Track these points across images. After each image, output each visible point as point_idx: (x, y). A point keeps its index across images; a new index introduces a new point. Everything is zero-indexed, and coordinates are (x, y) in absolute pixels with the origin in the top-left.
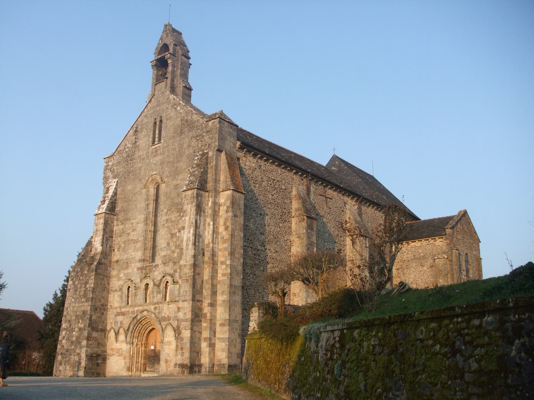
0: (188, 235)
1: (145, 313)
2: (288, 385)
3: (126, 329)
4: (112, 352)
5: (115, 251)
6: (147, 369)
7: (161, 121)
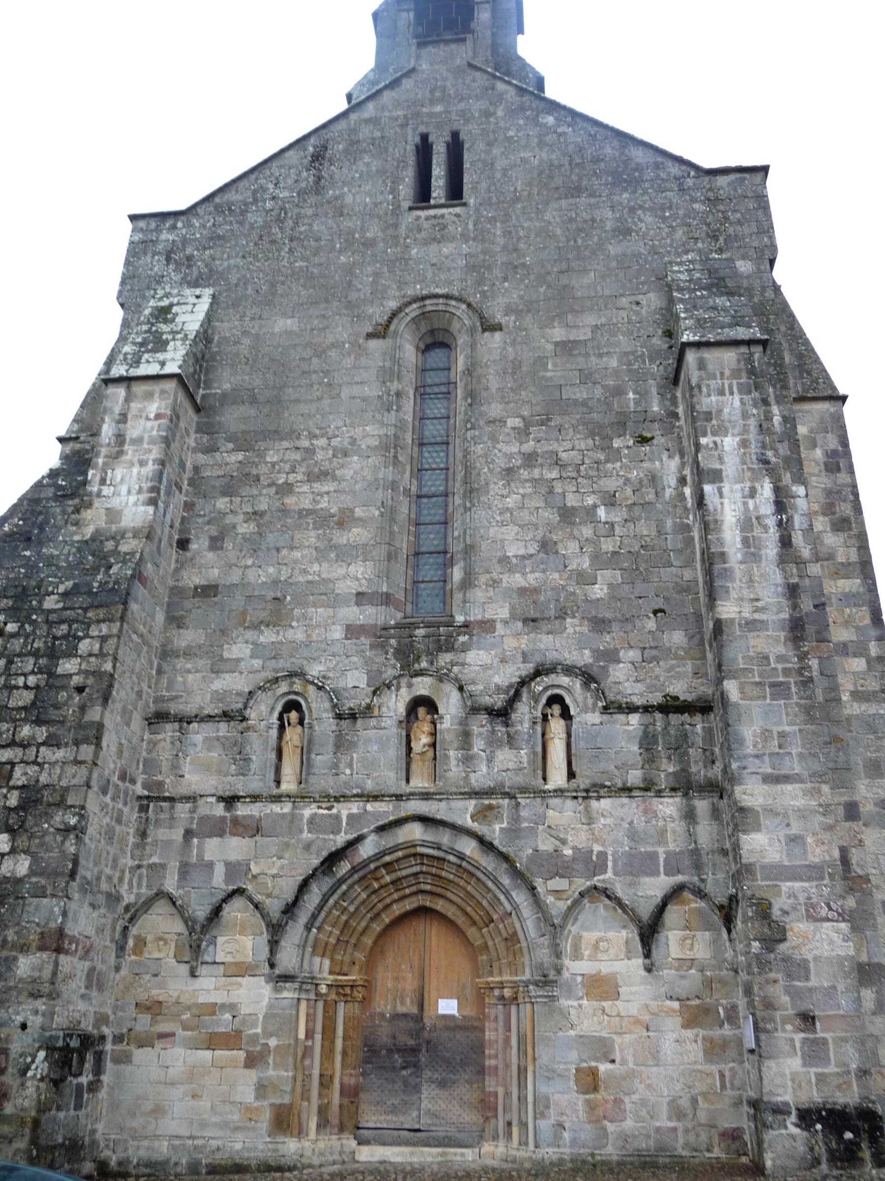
0: (745, 504)
1: (415, 832)
2: (281, 1106)
3: (274, 907)
4: (154, 1022)
5: (193, 546)
6: (371, 1118)
7: (456, 149)
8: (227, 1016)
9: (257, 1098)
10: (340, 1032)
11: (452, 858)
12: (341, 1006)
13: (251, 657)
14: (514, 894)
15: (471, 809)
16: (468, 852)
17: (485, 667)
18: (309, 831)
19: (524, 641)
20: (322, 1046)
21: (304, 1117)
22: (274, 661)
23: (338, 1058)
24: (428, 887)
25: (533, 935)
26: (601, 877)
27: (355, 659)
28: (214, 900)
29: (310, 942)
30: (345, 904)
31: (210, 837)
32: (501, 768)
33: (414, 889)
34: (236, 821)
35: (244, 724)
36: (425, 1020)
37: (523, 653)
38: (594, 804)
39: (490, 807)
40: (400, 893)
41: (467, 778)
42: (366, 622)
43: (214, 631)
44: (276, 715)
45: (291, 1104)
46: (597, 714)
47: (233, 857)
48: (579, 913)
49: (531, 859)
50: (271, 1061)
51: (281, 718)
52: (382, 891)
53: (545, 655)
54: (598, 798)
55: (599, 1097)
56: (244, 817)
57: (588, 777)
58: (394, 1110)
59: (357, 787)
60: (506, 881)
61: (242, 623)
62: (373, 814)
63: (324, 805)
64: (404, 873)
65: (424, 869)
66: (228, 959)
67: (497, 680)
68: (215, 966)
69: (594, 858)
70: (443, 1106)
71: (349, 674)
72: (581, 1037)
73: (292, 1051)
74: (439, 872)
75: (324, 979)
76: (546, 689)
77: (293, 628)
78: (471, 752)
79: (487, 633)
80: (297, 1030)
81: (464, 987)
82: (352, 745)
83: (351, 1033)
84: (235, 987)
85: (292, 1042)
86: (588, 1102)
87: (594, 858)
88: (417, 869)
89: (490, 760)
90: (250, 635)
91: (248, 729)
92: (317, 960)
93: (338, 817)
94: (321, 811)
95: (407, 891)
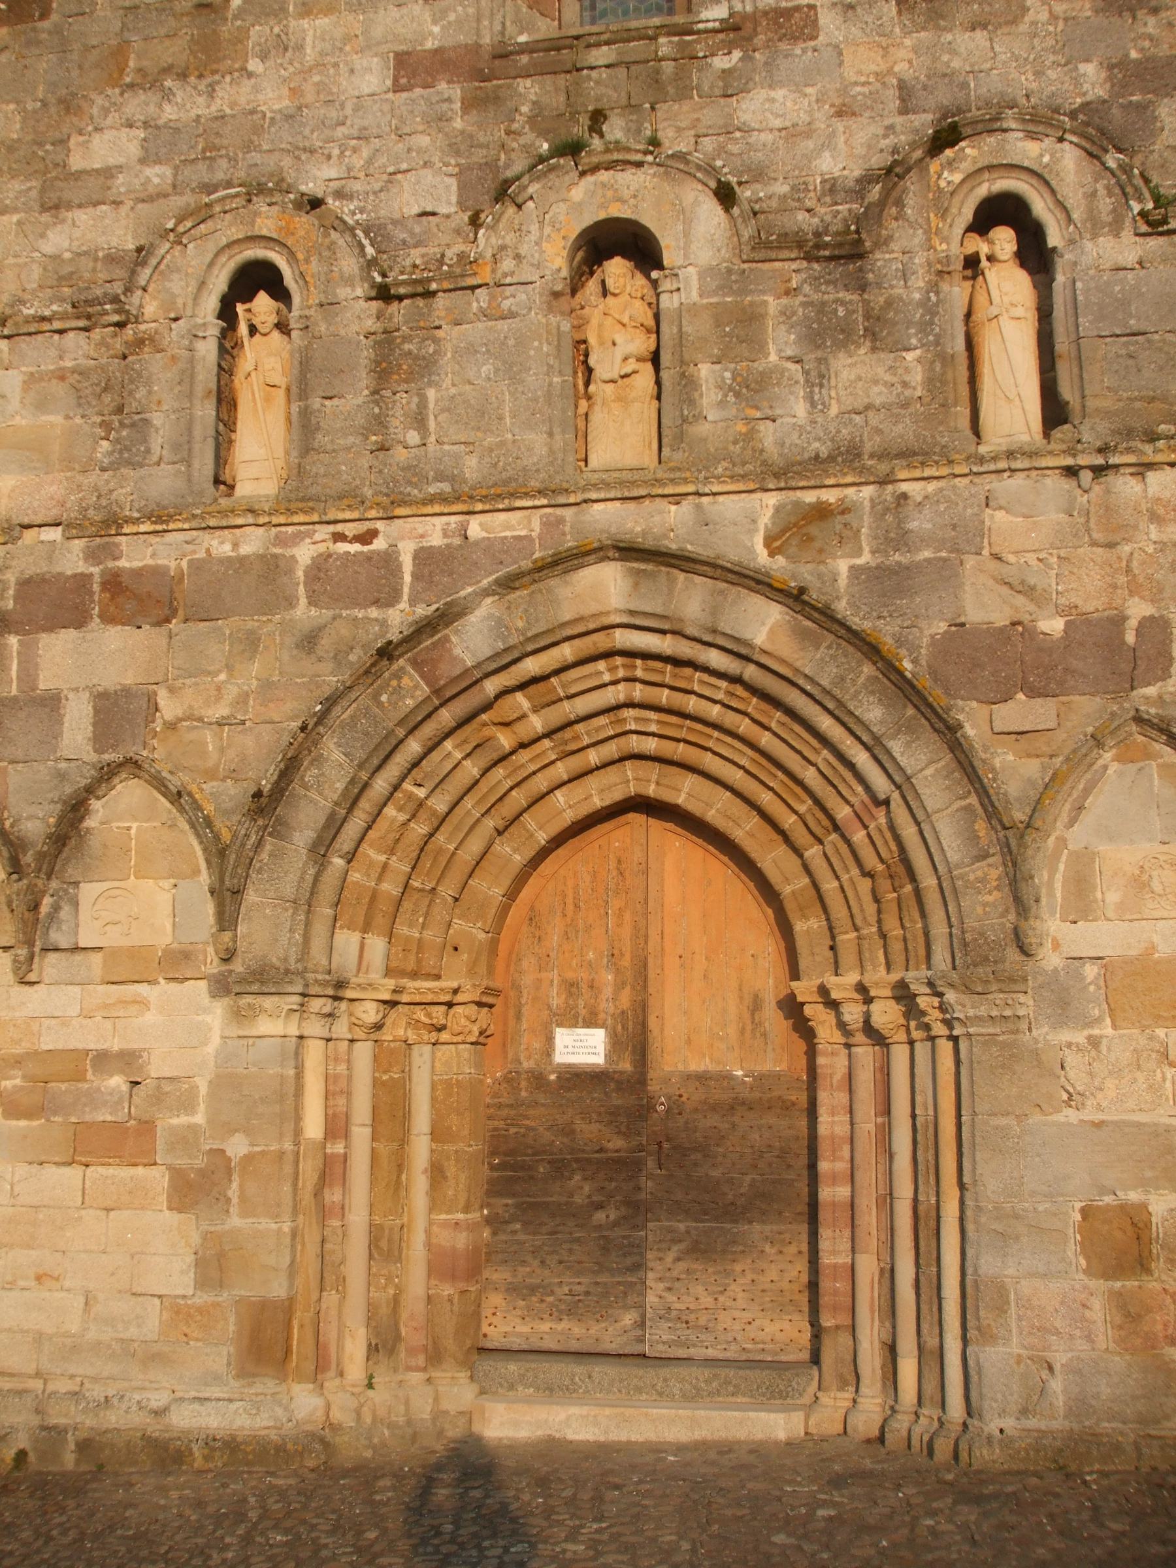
2: (264, 1305)
8: (117, 1082)
9: (202, 1283)
10: (422, 1121)
11: (715, 659)
12: (422, 1057)
13: (143, 161)
14: (896, 746)
15: (765, 519)
16: (760, 638)
17: (792, 133)
18: (313, 602)
19: (902, 53)
20: (374, 1156)
21: (330, 1333)
22: (202, 166)
23: (420, 1184)
24: (651, 745)
25: (953, 856)
26: (1151, 691)
27: (424, 141)
28: (68, 790)
29: (327, 890)
30: (421, 793)
31: (50, 629)
32: (849, 403)
33: (611, 750)
34: (114, 584)
35: (129, 331)
36: (653, 1087)
37: (902, 86)
38: (1126, 487)
39: (822, 512)
40: (575, 764)
41: (750, 436)
42: (449, 42)
43: (45, 104)
44: (211, 303)
45: (291, 1300)
46: (1127, 235)
47: (112, 677)
48: (1087, 792)
49: (944, 647)
50: (233, 1191)
51: (227, 312)
52: (524, 756)
53: (964, 86)
54: (1143, 468)
55: (1154, 1285)
56: (138, 573)
57: (1107, 414)
58: (572, 1309)
59: (440, 477)
60: (873, 712)
61: (114, 80)
62: (487, 546)
63: (350, 530)
64: (582, 705)
65: (638, 692)
66: (113, 938)
67: (829, 165)
68: (78, 957)
69: (1130, 638)
70: (707, 1301)
71: (405, 180)
72: (1099, 1125)
73: (288, 1169)
74: (678, 700)
75: (371, 986)
76: (973, 176)
77: (250, 75)
78: (760, 366)
79: (794, 39)
80: (298, 1118)
81: (756, 1005)
82: (425, 368)
83: (454, 1121)
84: (133, 1009)
85: (288, 1146)
86: (1120, 1301)
87: (1130, 638)
88: (619, 693)
89: (818, 379)
90: (138, 105)
91: (140, 343)
92: (347, 941)
93: (389, 560)
94: (343, 547)
95: (593, 757)
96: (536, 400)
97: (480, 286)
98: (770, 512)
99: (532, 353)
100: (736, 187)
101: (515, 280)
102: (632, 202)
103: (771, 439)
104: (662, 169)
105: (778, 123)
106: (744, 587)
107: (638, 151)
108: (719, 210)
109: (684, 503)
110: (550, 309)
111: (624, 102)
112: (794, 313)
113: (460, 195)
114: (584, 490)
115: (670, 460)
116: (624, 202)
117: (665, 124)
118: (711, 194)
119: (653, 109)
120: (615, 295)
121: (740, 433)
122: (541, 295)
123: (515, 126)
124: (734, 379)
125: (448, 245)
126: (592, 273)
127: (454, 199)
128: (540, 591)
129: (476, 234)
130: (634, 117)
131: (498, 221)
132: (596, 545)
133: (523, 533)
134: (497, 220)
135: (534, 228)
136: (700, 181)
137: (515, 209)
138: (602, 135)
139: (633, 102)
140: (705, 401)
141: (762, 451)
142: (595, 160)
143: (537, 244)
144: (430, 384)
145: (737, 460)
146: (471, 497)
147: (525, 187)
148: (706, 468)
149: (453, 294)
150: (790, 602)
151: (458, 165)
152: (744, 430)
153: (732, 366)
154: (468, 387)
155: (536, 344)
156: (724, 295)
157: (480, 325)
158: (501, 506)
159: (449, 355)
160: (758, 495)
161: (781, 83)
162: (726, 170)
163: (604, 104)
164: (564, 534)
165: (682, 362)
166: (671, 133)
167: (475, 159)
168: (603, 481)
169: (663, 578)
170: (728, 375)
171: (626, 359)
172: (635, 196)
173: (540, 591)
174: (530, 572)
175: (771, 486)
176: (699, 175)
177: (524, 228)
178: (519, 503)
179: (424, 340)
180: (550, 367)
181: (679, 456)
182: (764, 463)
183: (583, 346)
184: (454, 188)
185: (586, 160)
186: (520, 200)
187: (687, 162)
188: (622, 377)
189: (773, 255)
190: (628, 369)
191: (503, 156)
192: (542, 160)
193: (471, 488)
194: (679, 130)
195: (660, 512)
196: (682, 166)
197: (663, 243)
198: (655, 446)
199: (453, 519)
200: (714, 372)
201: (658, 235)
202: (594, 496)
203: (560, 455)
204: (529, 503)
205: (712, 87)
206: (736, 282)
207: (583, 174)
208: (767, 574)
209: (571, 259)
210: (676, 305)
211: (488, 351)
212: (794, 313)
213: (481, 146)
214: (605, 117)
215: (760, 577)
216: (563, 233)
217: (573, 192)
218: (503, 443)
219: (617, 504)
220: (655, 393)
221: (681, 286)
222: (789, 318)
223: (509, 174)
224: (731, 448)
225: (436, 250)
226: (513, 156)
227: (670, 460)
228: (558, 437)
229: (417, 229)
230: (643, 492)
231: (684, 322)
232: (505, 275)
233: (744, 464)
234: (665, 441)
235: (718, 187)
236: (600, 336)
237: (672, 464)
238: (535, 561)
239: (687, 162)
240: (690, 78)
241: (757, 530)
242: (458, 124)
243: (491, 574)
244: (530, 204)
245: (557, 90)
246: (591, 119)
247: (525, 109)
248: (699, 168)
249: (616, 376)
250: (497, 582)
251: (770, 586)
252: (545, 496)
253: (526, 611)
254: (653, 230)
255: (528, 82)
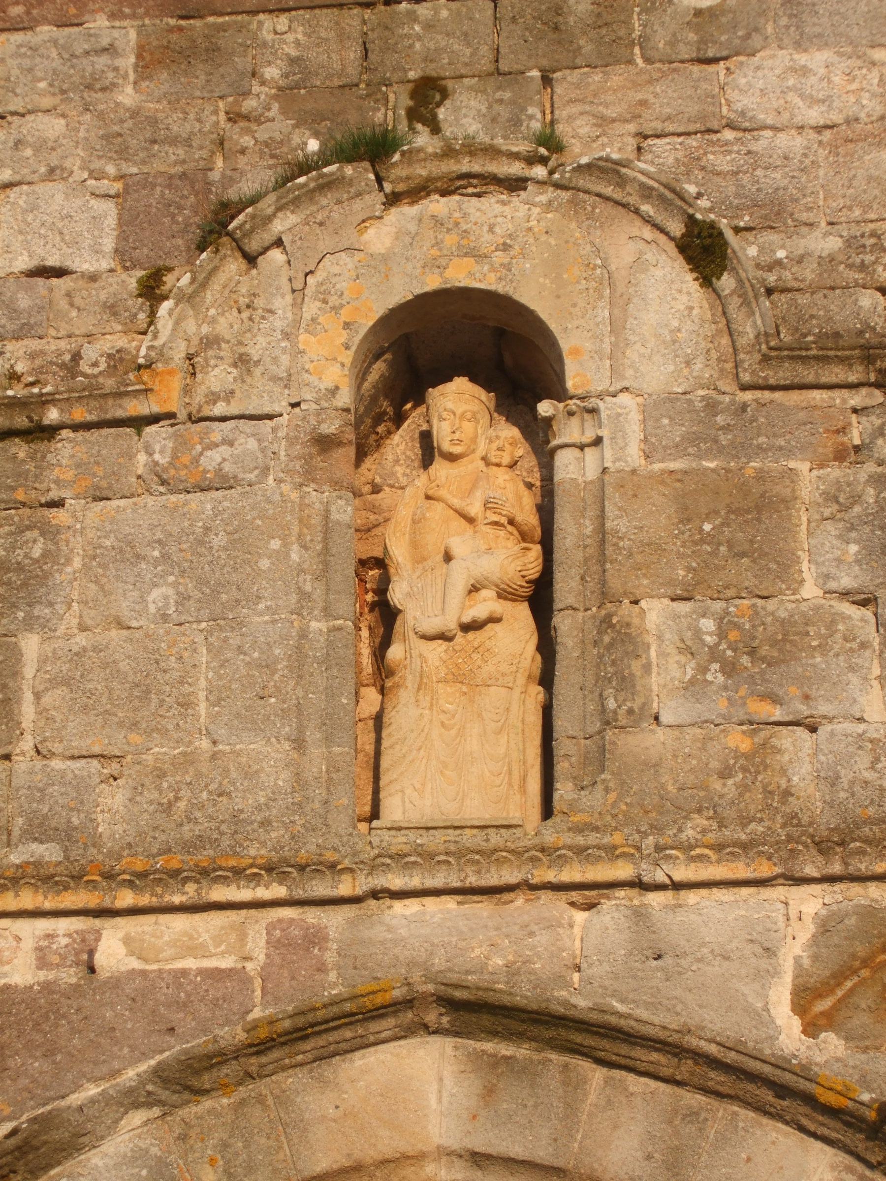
27: (53, 127)
96: (269, 666)
97: (154, 419)
98: (806, 932)
99: (264, 564)
100: (729, 234)
101: (234, 410)
102: (499, 257)
103: (806, 768)
104: (565, 195)
105: (815, 115)
106: (747, 1104)
107: (516, 156)
108: (689, 282)
109: (607, 905)
110: (309, 475)
111: (485, 64)
112: (856, 499)
113: (122, 237)
114: (373, 868)
115: (573, 807)
116: (480, 257)
117: (574, 109)
118: (671, 247)
119: (547, 81)
120: (452, 458)
121: (737, 754)
122: (291, 441)
123: (249, 104)
124: (722, 634)
125: (89, 336)
126: (399, 419)
127: (109, 243)
128: (261, 1100)
129: (152, 314)
130: (507, 95)
131: (204, 285)
132: (397, 993)
133: (226, 963)
134: (202, 284)
135: (282, 303)
136: (648, 221)
137: (242, 263)
138: (435, 129)
139: (504, 66)
140: (654, 680)
141: (787, 793)
142: (422, 171)
143: (286, 336)
144: (29, 624)
145: (730, 813)
146: (109, 876)
147: (269, 219)
148: (656, 828)
149: (94, 435)
150: (858, 1141)
151: (121, 177)
152: (745, 745)
153: (719, 606)
154: (114, 633)
155: (275, 544)
156: (699, 457)
157: (150, 500)
158: (177, 899)
159: (77, 563)
160: (779, 892)
161: (821, 41)
162: (703, 203)
163: (441, 67)
164: (322, 969)
165: (605, 596)
166: (584, 126)
167: (158, 166)
168: (419, 851)
169: (552, 1079)
170: (708, 625)
171: (474, 589)
172: (506, 247)
173: (261, 1100)
174: (238, 1053)
175: (810, 870)
176: (646, 208)
177: (259, 302)
178: (219, 893)
179: (22, 530)
180: (304, 596)
181: (594, 799)
182: (792, 819)
183: (374, 573)
184: (111, 221)
185: (401, 172)
186: (253, 245)
187: (622, 182)
188: (466, 628)
189: (809, 375)
190: (480, 610)
191: (219, 163)
192: (304, 168)
193: (110, 854)
194: (603, 122)
195: (551, 925)
196: (608, 191)
197: (565, 344)
198: (534, 785)
199: (64, 925)
200: (676, 617)
201: (553, 326)
202: (396, 882)
203: (318, 793)
204: (245, 894)
205: (673, 43)
206: (726, 428)
207: (393, 200)
208: (805, 1072)
209: (361, 376)
210: (592, 473)
211: (166, 557)
212: (856, 499)
213: (174, 141)
214: (445, 94)
215: (787, 1078)
216: (345, 315)
217: (371, 234)
218: (188, 759)
219: (450, 903)
220: (537, 671)
221: (604, 433)
222: (845, 508)
223: (232, 194)
224: (717, 785)
225: (63, 344)
226: (242, 162)
227: (573, 807)
228: (316, 752)
229: (24, 301)
230: (510, 876)
231: (611, 510)
232: (214, 398)
233: (745, 821)
234: (561, 767)
235: (687, 235)
236: (415, 544)
237: (576, 819)
238: (254, 1026)
239: (622, 182)
240: (627, 23)
241: (776, 973)
242: (127, 96)
243: (145, 1056)
244: (276, 255)
245: (342, 37)
246: (413, 95)
247: (272, 72)
248: (646, 192)
249: (450, 623)
250: (160, 1074)
251: (810, 1100)
252: (282, 878)
253: (225, 1145)
254: (543, 316)
255: (282, 22)
